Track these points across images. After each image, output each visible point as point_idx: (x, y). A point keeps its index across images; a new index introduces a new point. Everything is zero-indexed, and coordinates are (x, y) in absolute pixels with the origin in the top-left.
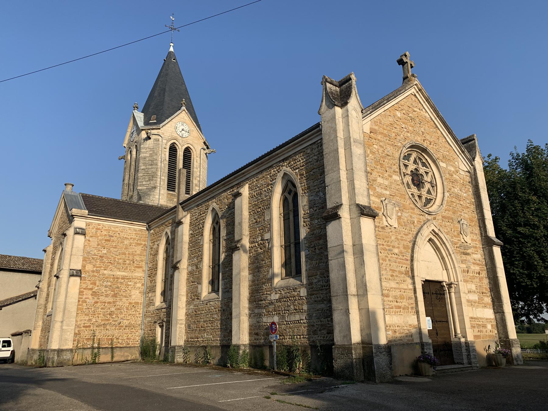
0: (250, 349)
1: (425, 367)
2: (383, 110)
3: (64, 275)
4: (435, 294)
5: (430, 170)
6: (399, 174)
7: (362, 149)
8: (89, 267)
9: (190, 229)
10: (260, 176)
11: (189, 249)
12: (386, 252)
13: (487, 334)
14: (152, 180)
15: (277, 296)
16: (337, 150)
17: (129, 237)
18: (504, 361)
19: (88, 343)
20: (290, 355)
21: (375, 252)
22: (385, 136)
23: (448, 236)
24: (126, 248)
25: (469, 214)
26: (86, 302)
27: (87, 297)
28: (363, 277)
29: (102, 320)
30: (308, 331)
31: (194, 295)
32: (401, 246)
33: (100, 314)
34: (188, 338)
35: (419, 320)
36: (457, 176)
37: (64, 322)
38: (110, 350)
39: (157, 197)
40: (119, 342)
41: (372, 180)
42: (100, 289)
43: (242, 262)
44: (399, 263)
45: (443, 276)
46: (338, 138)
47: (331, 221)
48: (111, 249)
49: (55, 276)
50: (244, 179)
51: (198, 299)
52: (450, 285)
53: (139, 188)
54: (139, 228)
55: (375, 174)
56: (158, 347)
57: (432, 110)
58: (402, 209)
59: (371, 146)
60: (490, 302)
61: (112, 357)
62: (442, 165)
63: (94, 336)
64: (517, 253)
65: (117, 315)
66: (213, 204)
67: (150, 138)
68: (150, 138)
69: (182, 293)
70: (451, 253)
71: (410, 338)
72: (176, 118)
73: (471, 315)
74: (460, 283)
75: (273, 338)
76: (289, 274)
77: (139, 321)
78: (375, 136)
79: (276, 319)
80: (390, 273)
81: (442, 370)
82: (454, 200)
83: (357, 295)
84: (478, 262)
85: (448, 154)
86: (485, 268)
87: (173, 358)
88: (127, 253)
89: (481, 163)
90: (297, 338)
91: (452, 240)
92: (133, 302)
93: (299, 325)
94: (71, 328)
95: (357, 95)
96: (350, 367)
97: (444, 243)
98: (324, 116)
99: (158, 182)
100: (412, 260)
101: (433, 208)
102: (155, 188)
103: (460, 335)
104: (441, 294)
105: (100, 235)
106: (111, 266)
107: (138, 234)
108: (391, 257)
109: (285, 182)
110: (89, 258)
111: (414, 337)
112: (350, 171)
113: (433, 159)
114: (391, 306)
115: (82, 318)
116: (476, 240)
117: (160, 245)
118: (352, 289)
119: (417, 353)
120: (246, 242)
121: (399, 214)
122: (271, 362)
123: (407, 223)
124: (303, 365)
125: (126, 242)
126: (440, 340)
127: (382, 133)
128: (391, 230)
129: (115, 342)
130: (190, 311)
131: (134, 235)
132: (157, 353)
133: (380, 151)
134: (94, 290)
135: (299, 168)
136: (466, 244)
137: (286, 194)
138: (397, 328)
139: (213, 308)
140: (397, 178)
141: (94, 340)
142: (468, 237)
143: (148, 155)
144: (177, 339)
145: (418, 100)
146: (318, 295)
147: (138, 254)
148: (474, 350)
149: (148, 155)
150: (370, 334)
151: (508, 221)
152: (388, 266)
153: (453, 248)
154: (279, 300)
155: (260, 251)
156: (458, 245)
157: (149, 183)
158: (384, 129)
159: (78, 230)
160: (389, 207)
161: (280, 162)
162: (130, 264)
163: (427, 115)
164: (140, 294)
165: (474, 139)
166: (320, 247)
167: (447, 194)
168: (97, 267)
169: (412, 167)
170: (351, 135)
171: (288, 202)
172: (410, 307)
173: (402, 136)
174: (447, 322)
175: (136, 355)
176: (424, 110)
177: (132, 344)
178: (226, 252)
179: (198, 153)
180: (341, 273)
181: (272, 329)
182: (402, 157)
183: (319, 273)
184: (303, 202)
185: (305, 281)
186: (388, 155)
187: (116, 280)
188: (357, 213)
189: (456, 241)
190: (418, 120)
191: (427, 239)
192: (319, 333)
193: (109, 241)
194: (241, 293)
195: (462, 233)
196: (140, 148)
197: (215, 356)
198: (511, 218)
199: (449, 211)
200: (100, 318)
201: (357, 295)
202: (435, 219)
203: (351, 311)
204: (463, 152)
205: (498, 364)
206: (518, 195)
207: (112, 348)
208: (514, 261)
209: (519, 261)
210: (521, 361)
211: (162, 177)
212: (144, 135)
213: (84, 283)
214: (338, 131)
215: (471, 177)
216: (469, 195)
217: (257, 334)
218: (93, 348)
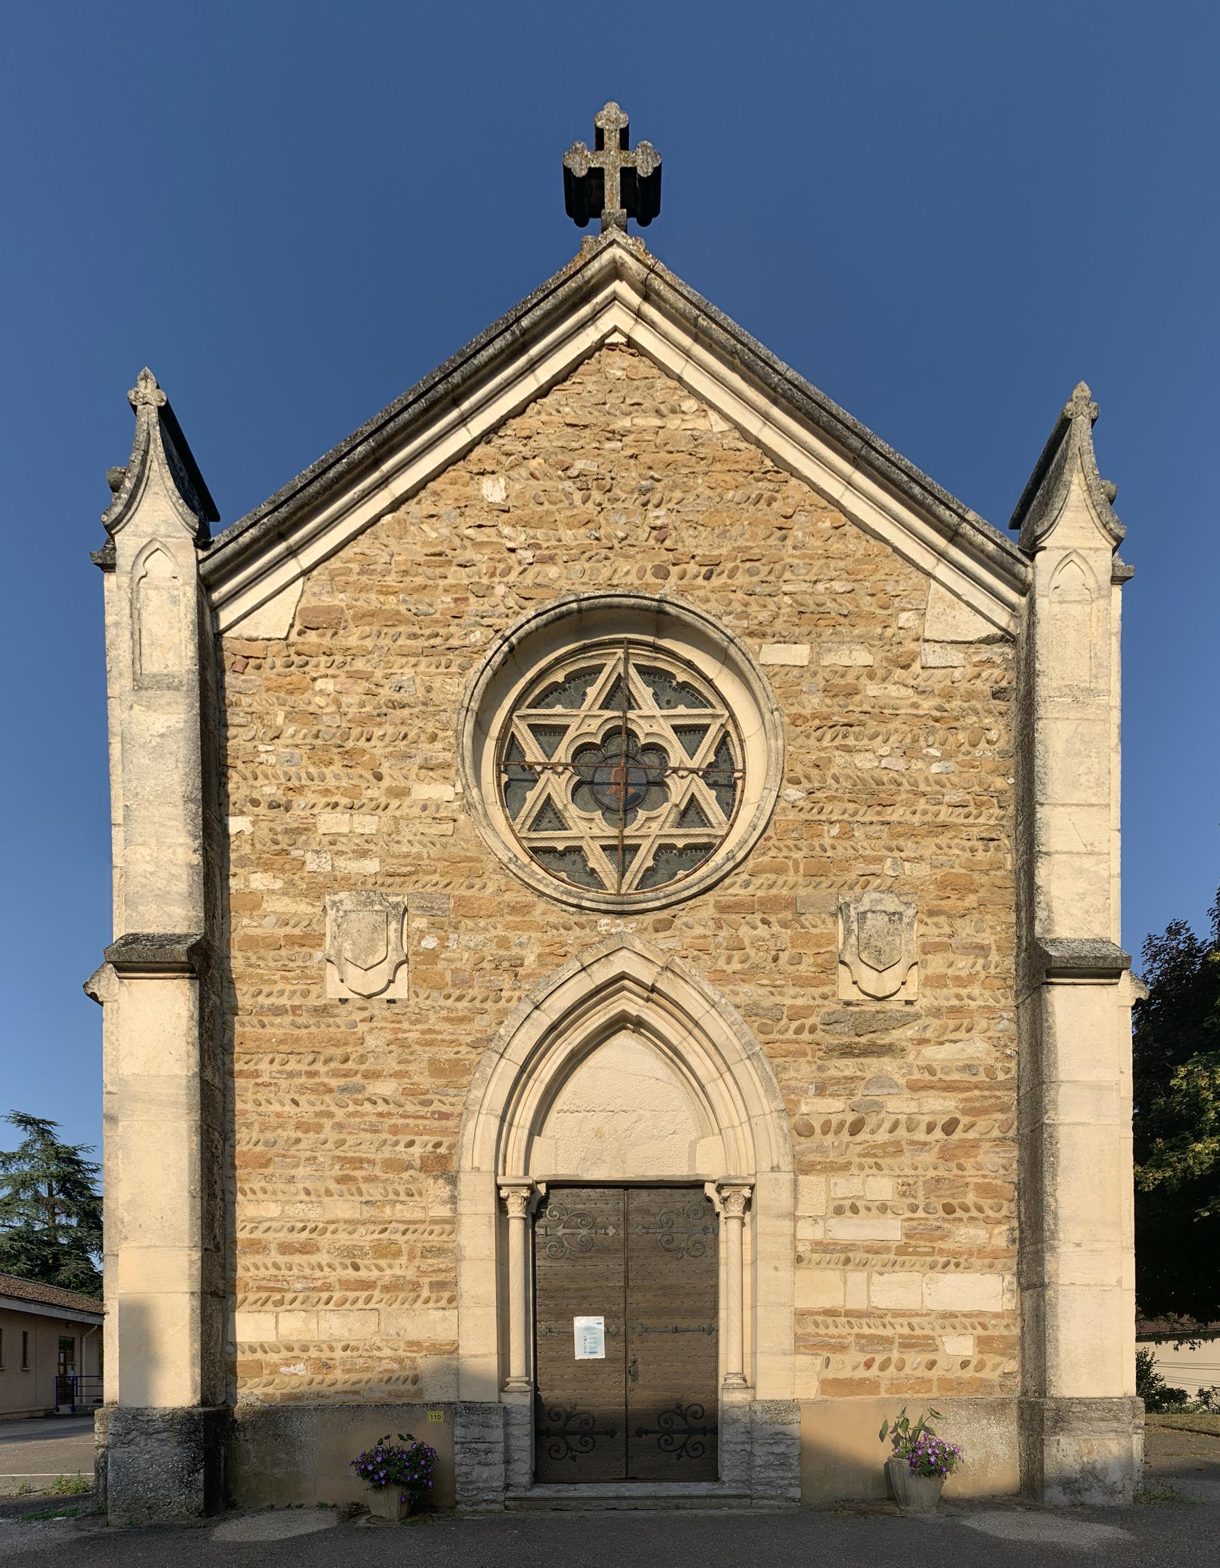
12: (327, 1098)
44: (395, 1133)
59: (304, 690)
71: (412, 1388)
138: (339, 1354)
156: (813, 1020)
176: (690, 405)
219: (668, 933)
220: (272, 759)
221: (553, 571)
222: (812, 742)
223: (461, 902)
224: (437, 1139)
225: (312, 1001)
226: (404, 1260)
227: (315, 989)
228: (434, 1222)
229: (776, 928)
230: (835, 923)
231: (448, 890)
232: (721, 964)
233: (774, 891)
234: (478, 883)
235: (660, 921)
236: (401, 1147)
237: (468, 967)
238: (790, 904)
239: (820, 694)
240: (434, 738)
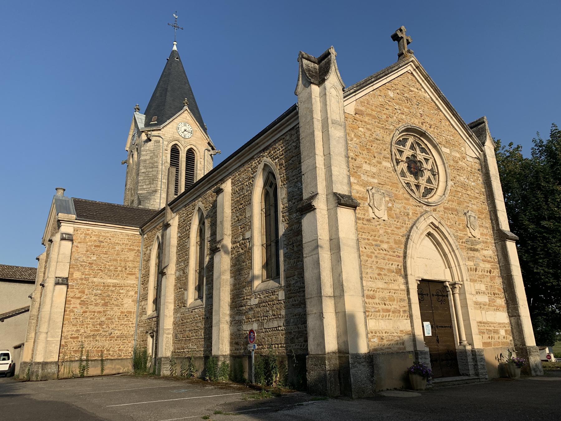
0: (230, 360)
1: (416, 379)
2: (371, 89)
3: (50, 283)
4: (435, 296)
5: (431, 156)
6: (390, 160)
7: (343, 131)
8: (77, 275)
9: (179, 232)
10: (242, 169)
11: (177, 253)
12: (372, 247)
13: (500, 340)
14: (153, 184)
15: (256, 301)
16: (313, 134)
17: (121, 243)
18: (518, 371)
19: (76, 355)
20: (267, 366)
21: (356, 247)
22: (374, 117)
23: (452, 230)
25: (478, 205)
26: (73, 312)
27: (75, 306)
28: (340, 275)
29: (91, 331)
30: (286, 339)
31: (180, 302)
32: (391, 241)
33: (89, 324)
34: (175, 349)
35: (412, 326)
36: (464, 165)
37: (49, 333)
38: (100, 362)
39: (158, 201)
40: (110, 354)
43: (224, 263)
44: (389, 260)
45: (445, 275)
46: (315, 120)
47: (306, 213)
48: (101, 255)
49: (41, 285)
50: (227, 173)
51: (184, 306)
52: (453, 285)
53: (139, 192)
54: (132, 232)
55: (359, 159)
56: (149, 358)
58: (394, 199)
59: (356, 129)
60: (504, 304)
61: (102, 370)
62: (445, 150)
63: (83, 348)
64: (541, 250)
66: (199, 204)
67: (150, 140)
68: (150, 140)
69: (170, 301)
70: (455, 248)
71: (402, 346)
72: (179, 118)
73: (479, 319)
74: (465, 282)
75: (251, 347)
76: (269, 277)
77: (132, 331)
78: (361, 118)
79: (255, 327)
80: (377, 271)
81: (441, 382)
82: (459, 189)
83: (334, 296)
84: (489, 259)
85: (452, 138)
86: (498, 266)
87: (160, 370)
89: (493, 148)
90: (275, 347)
91: (456, 234)
92: (126, 310)
93: (277, 332)
95: (337, 71)
96: (322, 379)
97: (446, 238)
98: (300, 96)
99: (159, 185)
100: (405, 257)
101: (434, 199)
102: (156, 191)
103: (466, 343)
104: (443, 296)
105: (89, 241)
106: (101, 273)
107: (131, 239)
108: (378, 253)
109: (266, 174)
110: (77, 266)
111: (406, 344)
112: (328, 156)
113: (434, 144)
114: (377, 309)
115: (69, 329)
116: (486, 235)
117: (152, 250)
118: (328, 289)
119: (410, 363)
120: (228, 242)
121: (390, 205)
122: (250, 375)
123: (399, 215)
124: (280, 378)
125: (118, 248)
126: (441, 347)
127: (370, 115)
128: (378, 223)
129: (106, 354)
130: (177, 319)
131: (126, 240)
132: (149, 364)
133: (367, 135)
134: (82, 299)
135: (278, 157)
136: (473, 239)
137: (268, 187)
138: (384, 335)
139: (197, 316)
140: (388, 164)
141: (82, 351)
142: (476, 231)
143: (148, 157)
144: (164, 350)
145: (416, 79)
146: (295, 298)
147: (131, 261)
148: (483, 359)
149: (148, 157)
150: (347, 341)
151: (531, 214)
152: (375, 263)
153: (457, 243)
154: (258, 305)
155: (242, 251)
156: (464, 240)
157: (149, 187)
159: (64, 235)
160: (377, 196)
161: (260, 152)
163: (426, 95)
164: (133, 303)
165: (484, 122)
166: (298, 243)
167: (450, 183)
169: (408, 152)
170: (329, 116)
171: (269, 196)
172: (401, 310)
173: (395, 118)
174: (451, 327)
175: (128, 368)
176: (422, 90)
177: (124, 356)
178: (210, 254)
179: (202, 154)
180: (316, 271)
181: (250, 338)
182: (394, 142)
183: (296, 273)
184: (282, 194)
185: (283, 283)
186: (377, 139)
187: (107, 288)
188: (334, 203)
189: (461, 235)
190: (415, 100)
191: (426, 233)
192: (296, 341)
193: (99, 246)
194: (221, 298)
195: (469, 226)
196: (140, 150)
197: (199, 368)
198: (534, 211)
199: (453, 202)
200: (89, 329)
201: (334, 296)
202: (435, 210)
203: (325, 315)
204: (470, 136)
205: (511, 375)
206: (540, 185)
207: (102, 360)
208: (537, 259)
209: (543, 258)
210: (541, 372)
211: (163, 181)
212: (144, 137)
213: (71, 292)
214: (314, 112)
215: (481, 164)
216: (478, 184)
217: (237, 343)
218: (81, 360)
220: (352, 146)
221: (404, 117)
224: (398, 263)
225: (366, 218)
226: (395, 302)
227: (367, 214)
228: (401, 290)
236: (390, 265)
240: (385, 150)
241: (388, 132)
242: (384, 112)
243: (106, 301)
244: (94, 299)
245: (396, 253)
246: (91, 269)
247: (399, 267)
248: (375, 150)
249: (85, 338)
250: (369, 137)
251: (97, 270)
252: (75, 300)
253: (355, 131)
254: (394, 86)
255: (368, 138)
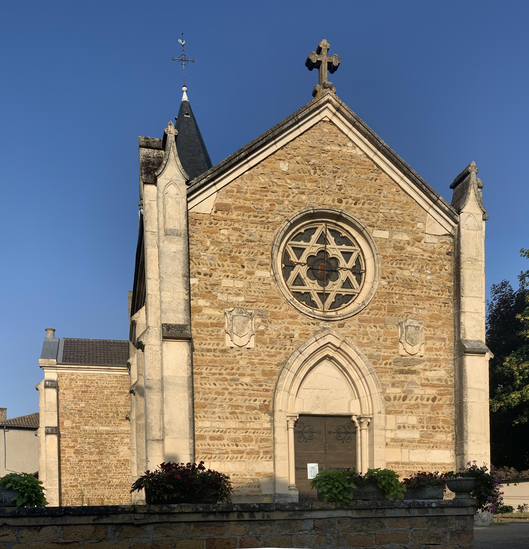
5: (357, 247)
8: (67, 423)
12: (226, 383)
17: (109, 386)
24: (107, 399)
26: (69, 461)
33: (86, 473)
41: (211, 285)
42: (82, 447)
48: (90, 401)
57: (366, 140)
63: (83, 496)
65: (105, 473)
71: (256, 489)
78: (225, 216)
84: (436, 382)
88: (109, 404)
92: (122, 459)
94: (55, 487)
104: (300, 432)
105: (76, 386)
106: (91, 421)
107: (121, 381)
108: (234, 389)
110: (67, 414)
114: (224, 451)
115: (68, 478)
121: (262, 328)
125: (106, 392)
131: (115, 382)
134: (76, 448)
141: (83, 499)
147: (122, 405)
152: (227, 400)
158: (246, 199)
162: (113, 417)
168: (76, 423)
169: (312, 247)
172: (262, 451)
176: (350, 144)
187: (99, 435)
193: (86, 392)
200: (87, 477)
204: (435, 202)
213: (64, 441)
219: (343, 328)
220: (206, 258)
221: (304, 197)
222: (389, 265)
223: (273, 313)
224: (264, 399)
225: (220, 347)
227: (221, 343)
229: (378, 329)
230: (398, 328)
231: (267, 309)
232: (361, 340)
233: (377, 316)
234: (279, 306)
235: (340, 324)
236: (252, 402)
237: (275, 337)
238: (383, 321)
239: (392, 248)
241: (271, 227)
242: (269, 198)
243: (101, 449)
244: (88, 448)
245: (264, 387)
246: (81, 416)
247: (266, 403)
248: (243, 258)
249: (84, 486)
250: (237, 240)
251: (88, 417)
252: (69, 449)
253: (214, 236)
254: (292, 152)
255: (234, 242)
